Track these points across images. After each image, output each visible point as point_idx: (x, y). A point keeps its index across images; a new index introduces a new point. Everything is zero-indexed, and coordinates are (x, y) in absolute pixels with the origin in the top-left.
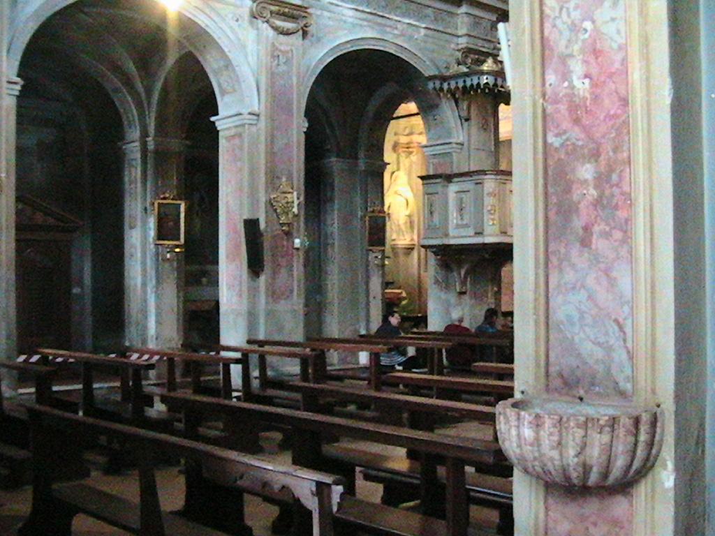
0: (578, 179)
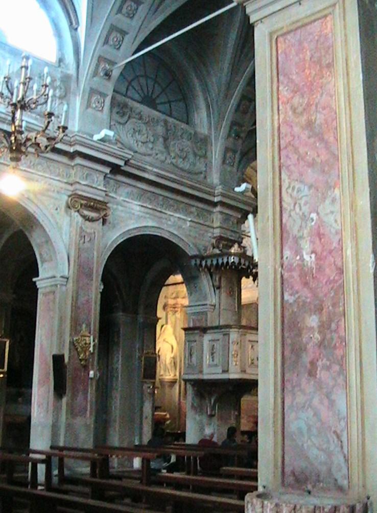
0: (307, 326)
